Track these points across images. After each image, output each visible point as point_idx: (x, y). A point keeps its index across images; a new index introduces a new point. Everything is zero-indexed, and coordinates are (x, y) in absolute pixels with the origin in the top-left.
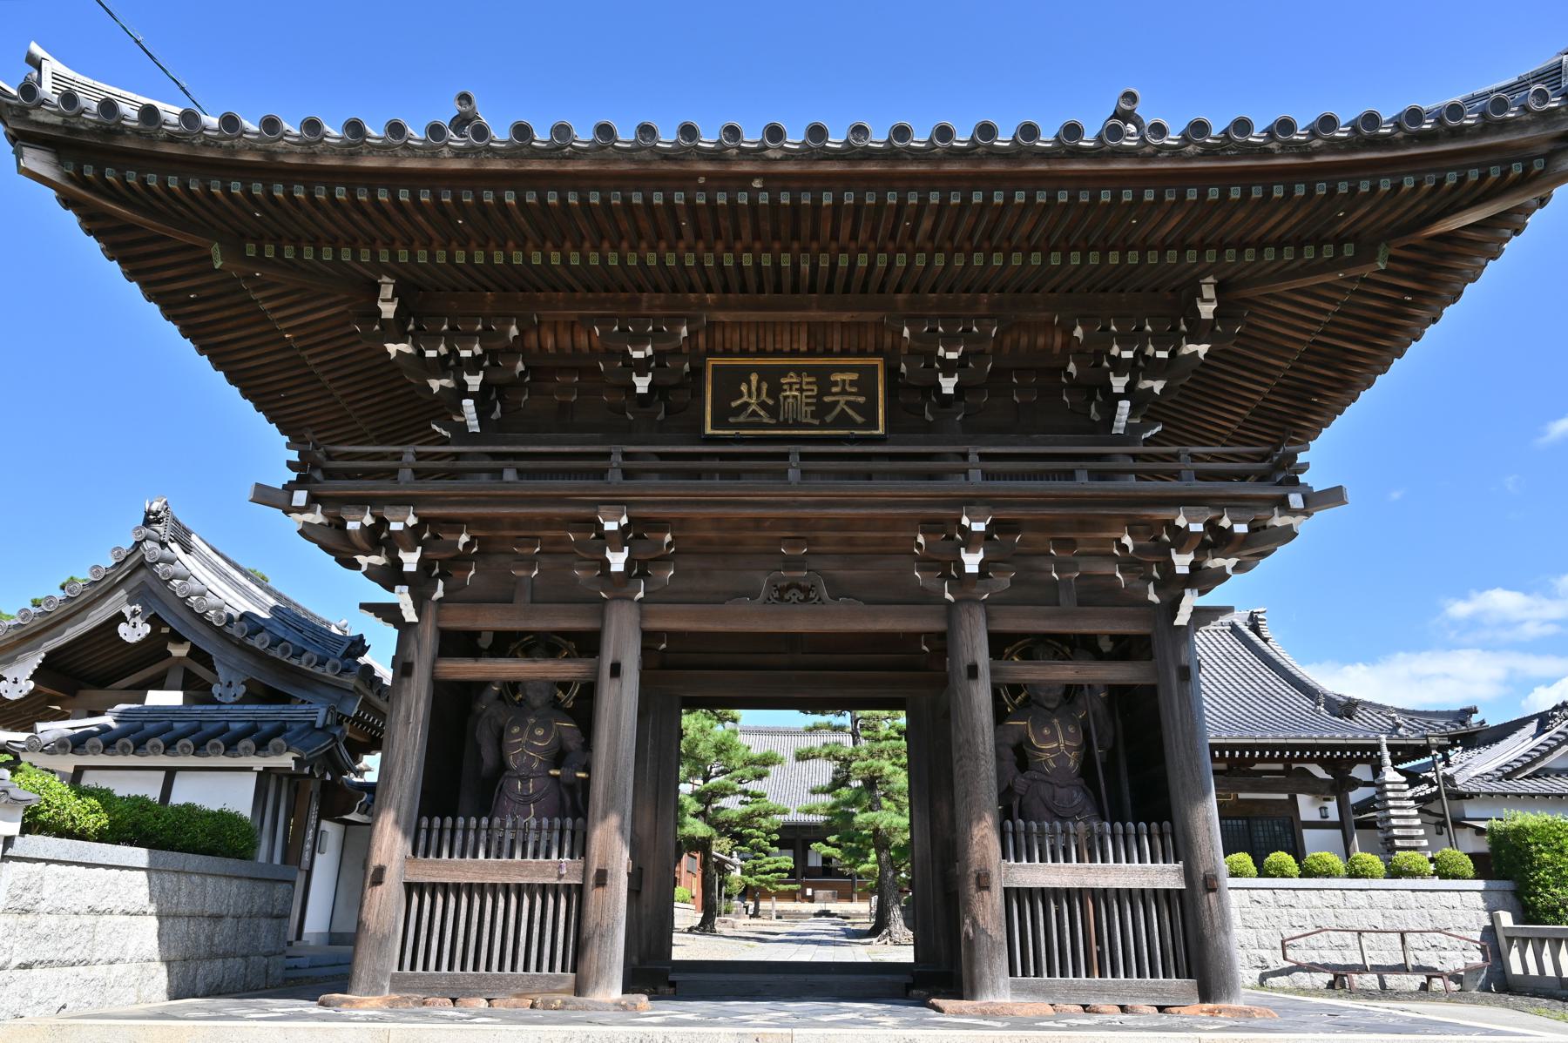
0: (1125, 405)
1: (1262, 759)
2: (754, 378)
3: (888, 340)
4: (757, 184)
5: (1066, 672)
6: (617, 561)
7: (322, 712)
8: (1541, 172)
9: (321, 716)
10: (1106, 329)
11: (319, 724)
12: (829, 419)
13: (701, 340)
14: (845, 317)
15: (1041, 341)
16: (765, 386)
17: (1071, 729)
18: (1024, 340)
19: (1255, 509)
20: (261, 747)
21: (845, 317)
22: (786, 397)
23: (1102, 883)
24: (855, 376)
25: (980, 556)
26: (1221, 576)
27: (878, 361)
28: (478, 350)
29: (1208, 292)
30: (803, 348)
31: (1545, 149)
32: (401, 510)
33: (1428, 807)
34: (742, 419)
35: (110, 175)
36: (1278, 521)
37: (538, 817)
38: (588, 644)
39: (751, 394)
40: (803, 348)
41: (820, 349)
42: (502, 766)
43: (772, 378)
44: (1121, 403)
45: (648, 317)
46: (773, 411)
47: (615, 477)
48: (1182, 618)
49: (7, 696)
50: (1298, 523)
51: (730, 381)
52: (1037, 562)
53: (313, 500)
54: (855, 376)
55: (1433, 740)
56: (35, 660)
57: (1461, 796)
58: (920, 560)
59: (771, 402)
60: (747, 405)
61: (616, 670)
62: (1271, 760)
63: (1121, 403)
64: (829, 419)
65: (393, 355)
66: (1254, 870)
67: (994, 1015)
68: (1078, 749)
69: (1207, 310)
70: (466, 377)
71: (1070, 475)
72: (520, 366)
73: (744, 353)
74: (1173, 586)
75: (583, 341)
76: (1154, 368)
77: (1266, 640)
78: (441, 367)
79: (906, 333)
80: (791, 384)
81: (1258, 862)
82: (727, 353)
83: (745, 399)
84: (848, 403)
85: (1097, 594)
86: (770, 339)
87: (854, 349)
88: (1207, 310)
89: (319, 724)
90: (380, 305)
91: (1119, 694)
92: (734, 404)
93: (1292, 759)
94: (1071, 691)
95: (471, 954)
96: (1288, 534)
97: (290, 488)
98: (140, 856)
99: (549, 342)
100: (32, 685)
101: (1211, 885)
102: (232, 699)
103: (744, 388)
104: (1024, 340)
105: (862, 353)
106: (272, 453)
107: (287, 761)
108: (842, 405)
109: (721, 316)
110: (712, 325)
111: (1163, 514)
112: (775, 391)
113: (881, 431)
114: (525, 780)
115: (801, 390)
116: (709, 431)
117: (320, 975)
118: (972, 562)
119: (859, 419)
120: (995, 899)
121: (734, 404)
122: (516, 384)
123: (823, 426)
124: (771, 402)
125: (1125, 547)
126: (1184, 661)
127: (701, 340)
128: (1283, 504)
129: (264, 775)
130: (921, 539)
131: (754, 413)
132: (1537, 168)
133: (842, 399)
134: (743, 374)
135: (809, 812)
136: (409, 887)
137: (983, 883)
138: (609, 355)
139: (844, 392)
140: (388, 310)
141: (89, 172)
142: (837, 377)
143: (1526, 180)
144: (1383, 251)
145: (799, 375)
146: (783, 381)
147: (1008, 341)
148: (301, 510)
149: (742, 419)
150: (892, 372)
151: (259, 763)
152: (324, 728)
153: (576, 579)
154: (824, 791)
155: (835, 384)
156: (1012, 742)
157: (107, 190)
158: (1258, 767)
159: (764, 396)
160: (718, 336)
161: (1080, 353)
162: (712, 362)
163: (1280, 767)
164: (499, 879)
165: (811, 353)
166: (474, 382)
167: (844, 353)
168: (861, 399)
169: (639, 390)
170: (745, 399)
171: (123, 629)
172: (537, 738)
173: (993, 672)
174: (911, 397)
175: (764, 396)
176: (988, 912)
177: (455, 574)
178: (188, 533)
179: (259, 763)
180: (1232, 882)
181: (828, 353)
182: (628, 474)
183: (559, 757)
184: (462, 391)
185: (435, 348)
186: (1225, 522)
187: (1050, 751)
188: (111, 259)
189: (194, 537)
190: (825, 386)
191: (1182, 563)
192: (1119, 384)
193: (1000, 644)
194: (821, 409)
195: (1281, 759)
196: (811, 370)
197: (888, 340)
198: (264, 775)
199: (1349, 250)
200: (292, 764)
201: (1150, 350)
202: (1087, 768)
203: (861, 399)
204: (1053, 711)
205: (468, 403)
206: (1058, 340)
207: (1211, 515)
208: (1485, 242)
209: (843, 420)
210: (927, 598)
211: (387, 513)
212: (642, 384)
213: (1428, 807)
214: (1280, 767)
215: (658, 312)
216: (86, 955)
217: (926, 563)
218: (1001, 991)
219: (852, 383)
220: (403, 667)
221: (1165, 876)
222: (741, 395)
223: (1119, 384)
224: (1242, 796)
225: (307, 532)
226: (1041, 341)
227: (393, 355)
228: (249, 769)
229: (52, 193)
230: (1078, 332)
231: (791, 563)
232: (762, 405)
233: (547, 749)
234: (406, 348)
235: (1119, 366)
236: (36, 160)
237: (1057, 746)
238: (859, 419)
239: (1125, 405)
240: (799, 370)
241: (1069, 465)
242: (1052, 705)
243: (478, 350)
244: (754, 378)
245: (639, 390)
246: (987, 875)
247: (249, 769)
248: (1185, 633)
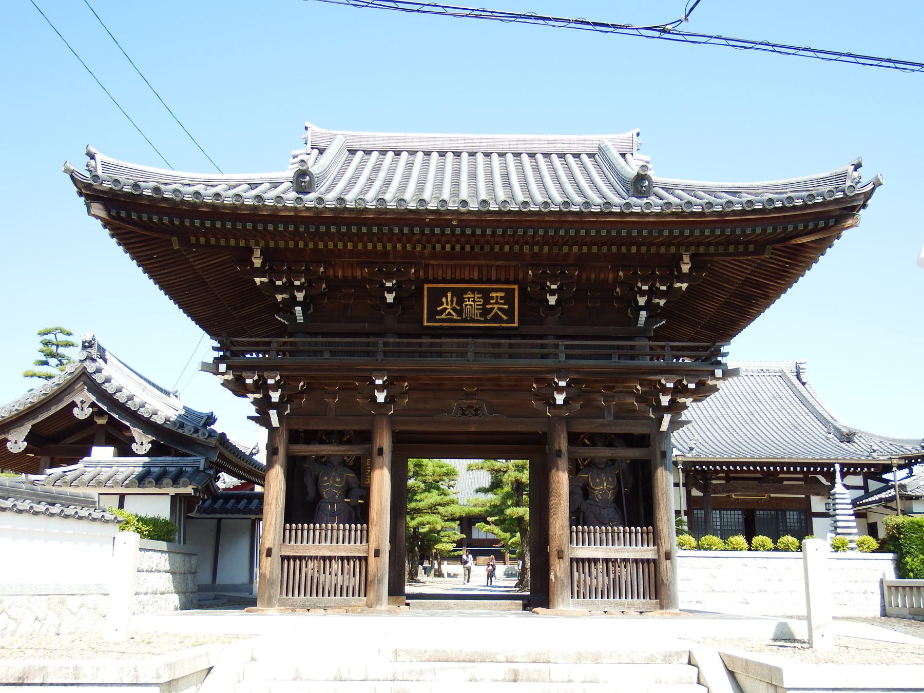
0: (643, 314)
1: (782, 472)
2: (449, 295)
3: (521, 275)
4: (454, 223)
5: (605, 453)
6: (381, 397)
7: (203, 461)
8: (832, 226)
9: (202, 463)
10: (636, 273)
11: (202, 468)
12: (489, 317)
13: (422, 273)
14: (498, 263)
15: (602, 276)
16: (455, 299)
17: (610, 479)
18: (593, 276)
19: (698, 376)
20: (175, 482)
21: (498, 263)
22: (466, 305)
23: (612, 555)
24: (503, 294)
25: (564, 396)
26: (684, 407)
27: (516, 287)
28: (303, 280)
29: (686, 259)
30: (476, 278)
31: (837, 213)
32: (272, 374)
33: (889, 504)
34: (443, 316)
35: (134, 216)
36: (711, 382)
37: (338, 524)
38: (366, 437)
39: (448, 304)
40: (476, 278)
41: (485, 279)
42: (319, 496)
43: (459, 295)
44: (642, 312)
45: (392, 263)
46: (459, 312)
47: (380, 357)
48: (664, 427)
49: (12, 451)
50: (720, 384)
51: (436, 297)
52: (594, 396)
53: (228, 368)
54: (503, 294)
55: (895, 461)
56: (26, 429)
57: (910, 498)
58: (535, 395)
59: (458, 308)
60: (446, 309)
61: (381, 452)
62: (795, 472)
63: (642, 312)
64: (489, 317)
65: (258, 284)
66: (746, 546)
67: (561, 615)
68: (614, 489)
69: (686, 268)
70: (296, 293)
71: (609, 357)
72: (324, 286)
73: (444, 281)
74: (660, 410)
75: (358, 274)
76: (662, 294)
77: (804, 384)
78: (280, 290)
79: (530, 272)
80: (469, 298)
81: (749, 541)
82: (435, 281)
83: (445, 306)
84: (499, 309)
85: (624, 413)
86: (458, 273)
87: (503, 279)
88: (686, 268)
89: (202, 468)
90: (253, 260)
91: (634, 463)
92: (439, 309)
93: (809, 471)
94: (613, 461)
95: (314, 588)
96: (715, 389)
97: (218, 361)
98: (163, 545)
99: (340, 274)
100: (25, 443)
101: (668, 556)
102: (144, 452)
103: (444, 300)
104: (593, 276)
105: (507, 282)
106: (205, 346)
107: (189, 490)
108: (495, 310)
109: (432, 262)
110: (427, 266)
111: (657, 378)
112: (460, 302)
113: (516, 325)
114: (332, 505)
115: (474, 301)
116: (425, 324)
117: (240, 598)
118: (560, 399)
119: (505, 318)
120: (566, 563)
121: (439, 309)
122: (322, 295)
123: (486, 321)
124: (458, 308)
125: (638, 390)
126: (663, 449)
127: (422, 273)
128: (712, 373)
129: (174, 498)
130: (535, 386)
131: (449, 314)
132: (831, 224)
133: (496, 306)
134: (444, 292)
135: (475, 505)
136: (283, 558)
137: (560, 556)
138: (371, 281)
139: (497, 303)
140: (257, 263)
141: (123, 214)
142: (494, 295)
143: (827, 228)
144: (769, 249)
145: (473, 293)
146: (465, 296)
147: (584, 276)
148: (223, 374)
149: (443, 316)
150: (522, 291)
151: (173, 491)
152: (203, 471)
153: (358, 403)
154: (485, 491)
155: (493, 298)
156: (580, 484)
157: (129, 220)
158: (781, 476)
159: (454, 305)
160: (431, 272)
161: (622, 283)
162: (426, 286)
163: (801, 476)
164: (328, 554)
165: (480, 281)
166: (300, 296)
167: (498, 281)
168: (506, 307)
169: (388, 301)
170: (445, 306)
171: (76, 411)
172: (337, 483)
173: (569, 452)
174: (532, 302)
175: (454, 305)
176: (559, 570)
177: (296, 401)
178: (104, 350)
179: (173, 491)
180: (680, 553)
181: (489, 281)
182: (385, 353)
183: (347, 492)
184: (293, 301)
185: (281, 280)
186: (685, 382)
187: (600, 490)
188: (133, 259)
189: (107, 353)
190: (487, 299)
191: (665, 400)
192: (642, 301)
193: (574, 439)
194: (485, 312)
195: (802, 472)
196: (480, 291)
197: (521, 275)
198: (174, 498)
199: (751, 248)
200: (192, 492)
201: (658, 285)
202: (618, 499)
203: (506, 307)
204: (602, 469)
205: (298, 309)
206: (611, 277)
207: (678, 378)
208: (821, 246)
209: (497, 318)
210: (537, 414)
211: (266, 374)
212: (390, 298)
213: (889, 504)
214: (801, 476)
215: (399, 260)
216: (31, 598)
217: (537, 396)
218: (564, 603)
219: (501, 298)
220: (272, 451)
221: (647, 552)
222: (443, 304)
223: (642, 301)
224: (772, 495)
225: (226, 384)
226: (602, 276)
227: (258, 284)
228: (167, 494)
229: (99, 222)
230: (621, 274)
231: (468, 395)
232: (454, 309)
233: (342, 488)
234: (265, 280)
235: (643, 293)
236: (83, 199)
237: (603, 487)
238: (505, 318)
239: (643, 314)
240: (473, 291)
241: (609, 352)
242: (602, 466)
243: (303, 280)
244: (449, 295)
245: (388, 301)
246: (562, 551)
247: (167, 494)
248: (666, 435)
